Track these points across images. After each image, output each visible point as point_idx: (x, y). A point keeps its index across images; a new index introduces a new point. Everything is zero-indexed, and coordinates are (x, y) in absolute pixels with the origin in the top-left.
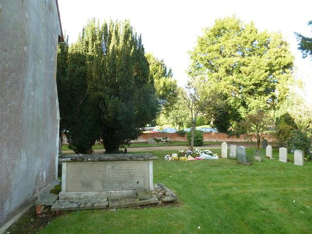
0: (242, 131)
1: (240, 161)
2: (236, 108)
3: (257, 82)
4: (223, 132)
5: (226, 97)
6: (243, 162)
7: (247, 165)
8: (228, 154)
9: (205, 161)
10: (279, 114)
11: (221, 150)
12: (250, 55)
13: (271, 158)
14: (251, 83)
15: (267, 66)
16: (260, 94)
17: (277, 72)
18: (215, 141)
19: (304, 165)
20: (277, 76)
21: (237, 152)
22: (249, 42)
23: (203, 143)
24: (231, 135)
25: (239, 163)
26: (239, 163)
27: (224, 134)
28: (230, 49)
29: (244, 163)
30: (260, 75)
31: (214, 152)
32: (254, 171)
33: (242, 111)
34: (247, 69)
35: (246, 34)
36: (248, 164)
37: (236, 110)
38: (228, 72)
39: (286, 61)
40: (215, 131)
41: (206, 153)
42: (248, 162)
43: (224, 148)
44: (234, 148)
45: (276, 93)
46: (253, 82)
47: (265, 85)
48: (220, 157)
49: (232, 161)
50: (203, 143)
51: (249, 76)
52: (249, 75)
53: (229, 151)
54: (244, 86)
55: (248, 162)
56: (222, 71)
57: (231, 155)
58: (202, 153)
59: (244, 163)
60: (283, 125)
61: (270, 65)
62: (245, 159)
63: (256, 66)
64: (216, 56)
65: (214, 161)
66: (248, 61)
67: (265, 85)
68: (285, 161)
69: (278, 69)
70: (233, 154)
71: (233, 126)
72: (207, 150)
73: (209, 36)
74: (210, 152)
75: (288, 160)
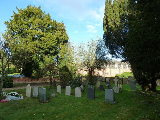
0: (40, 75)
1: (41, 99)
2: (37, 62)
3: (50, 47)
4: (28, 77)
5: (31, 54)
6: (44, 100)
7: (46, 102)
8: (32, 93)
9: (12, 102)
10: (61, 66)
11: (25, 90)
12: (47, 32)
13: (60, 93)
14: (47, 47)
15: (56, 39)
16: (51, 54)
17: (60, 44)
18: (22, 83)
19: (82, 96)
20: (60, 46)
21: (39, 91)
22: (47, 24)
23: (13, 85)
24: (33, 78)
25: (41, 102)
26: (41, 102)
27: (29, 78)
28: (36, 25)
29: (45, 101)
30: (52, 43)
31: (19, 92)
32: (53, 109)
33: (40, 63)
34: (45, 39)
35: (46, 19)
36: (47, 101)
37: (37, 63)
38: (34, 39)
39: (65, 39)
40: (23, 76)
41: (12, 95)
42: (47, 100)
43: (28, 88)
44: (36, 89)
45: (59, 55)
46: (48, 46)
47: (54, 49)
48: (25, 97)
49: (35, 99)
50: (13, 85)
51: (46, 43)
52: (46, 43)
53: (32, 90)
54: (43, 49)
55: (47, 100)
56: (29, 38)
57: (34, 94)
58: (8, 95)
59: (45, 101)
60: (64, 72)
61: (57, 39)
62: (45, 98)
63: (50, 38)
64: (27, 28)
65: (18, 101)
66: (46, 35)
67: (54, 49)
68: (69, 95)
69: (61, 42)
70: (36, 94)
71: (34, 73)
72: (14, 92)
73: (23, 15)
74: (16, 93)
75: (71, 94)
